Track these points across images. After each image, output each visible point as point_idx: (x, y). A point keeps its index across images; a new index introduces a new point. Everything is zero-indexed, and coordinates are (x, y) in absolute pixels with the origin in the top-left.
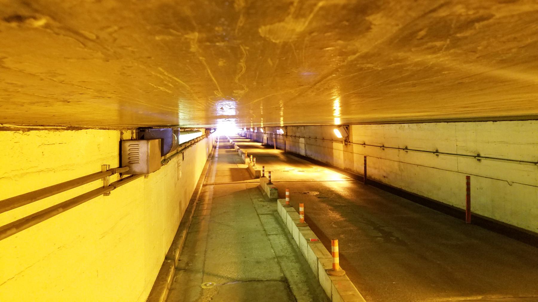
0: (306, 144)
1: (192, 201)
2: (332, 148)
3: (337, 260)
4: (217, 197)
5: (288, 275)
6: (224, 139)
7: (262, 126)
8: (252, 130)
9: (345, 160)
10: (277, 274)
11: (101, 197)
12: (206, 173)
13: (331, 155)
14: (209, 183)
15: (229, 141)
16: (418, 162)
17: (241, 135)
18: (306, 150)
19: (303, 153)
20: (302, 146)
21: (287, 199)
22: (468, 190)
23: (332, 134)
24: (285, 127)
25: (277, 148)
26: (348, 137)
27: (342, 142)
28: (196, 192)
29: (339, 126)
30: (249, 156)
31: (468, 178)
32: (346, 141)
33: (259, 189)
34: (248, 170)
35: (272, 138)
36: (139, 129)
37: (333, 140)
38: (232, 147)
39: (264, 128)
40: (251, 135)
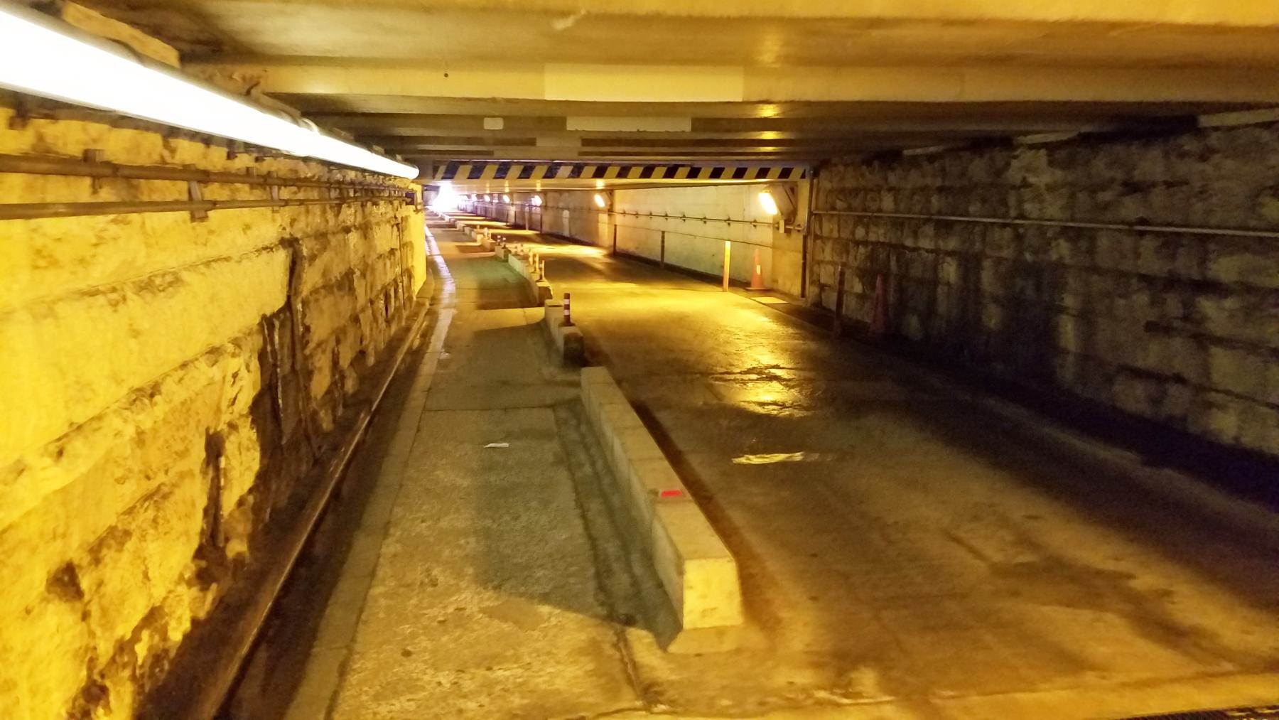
0: (571, 219)
2: (597, 221)
7: (507, 190)
8: (487, 198)
13: (596, 232)
17: (464, 210)
19: (566, 233)
20: (566, 222)
26: (612, 205)
29: (601, 191)
36: (836, 152)
38: (452, 225)
39: (511, 194)
40: (486, 209)
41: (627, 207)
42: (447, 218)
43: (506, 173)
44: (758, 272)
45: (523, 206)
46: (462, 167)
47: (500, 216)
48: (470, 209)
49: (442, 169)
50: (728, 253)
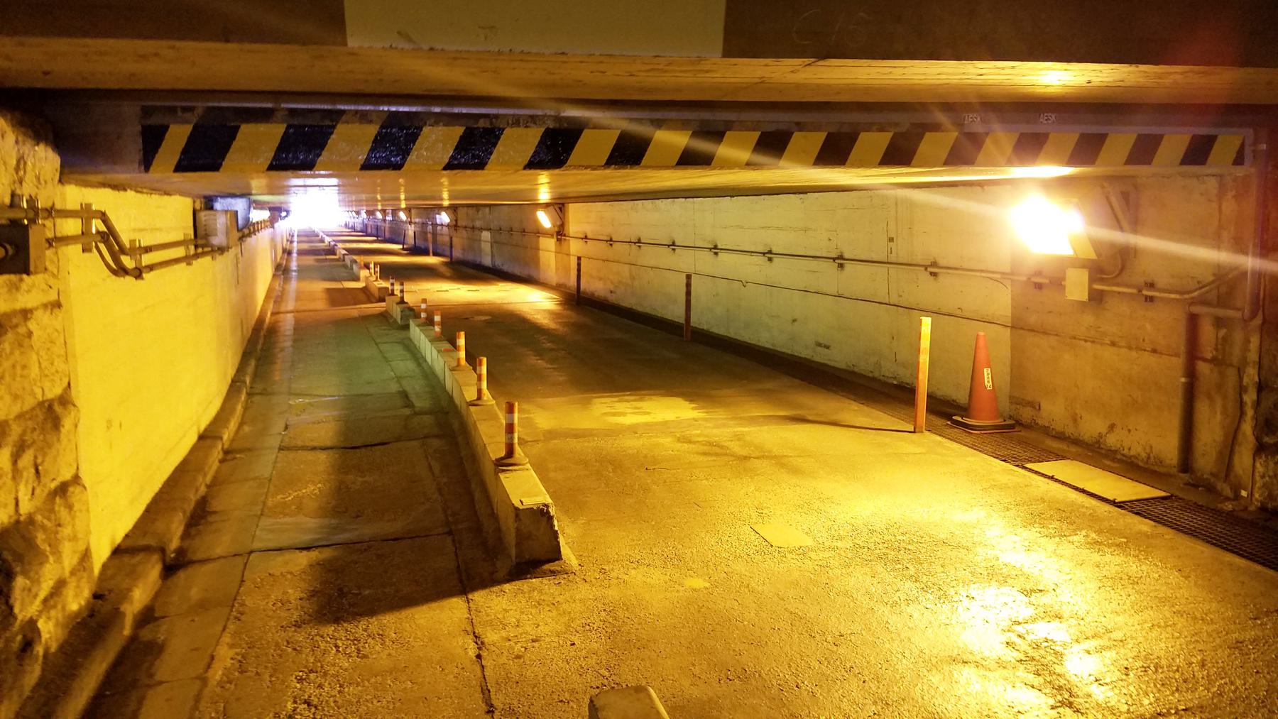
0: (494, 243)
1: (254, 330)
3: (462, 354)
4: (306, 330)
5: (408, 389)
6: (310, 236)
7: (403, 205)
8: (379, 215)
9: (557, 269)
10: (394, 387)
11: (183, 265)
12: (275, 296)
13: (536, 261)
14: (283, 309)
15: (322, 241)
16: (653, 263)
18: (493, 256)
19: (487, 261)
20: (486, 247)
21: (437, 329)
22: (688, 293)
23: (536, 221)
24: (453, 209)
25: (435, 254)
26: (562, 226)
27: (552, 236)
28: (260, 321)
30: (367, 266)
31: (689, 277)
32: (559, 233)
33: (384, 317)
34: (365, 290)
35: (426, 233)
37: (539, 232)
38: (331, 251)
39: (408, 210)
40: (377, 228)
41: (589, 229)
42: (327, 239)
43: (406, 153)
44: (988, 383)
45: (424, 224)
46: (247, 131)
47: (395, 235)
48: (359, 227)
49: (178, 136)
50: (925, 343)
